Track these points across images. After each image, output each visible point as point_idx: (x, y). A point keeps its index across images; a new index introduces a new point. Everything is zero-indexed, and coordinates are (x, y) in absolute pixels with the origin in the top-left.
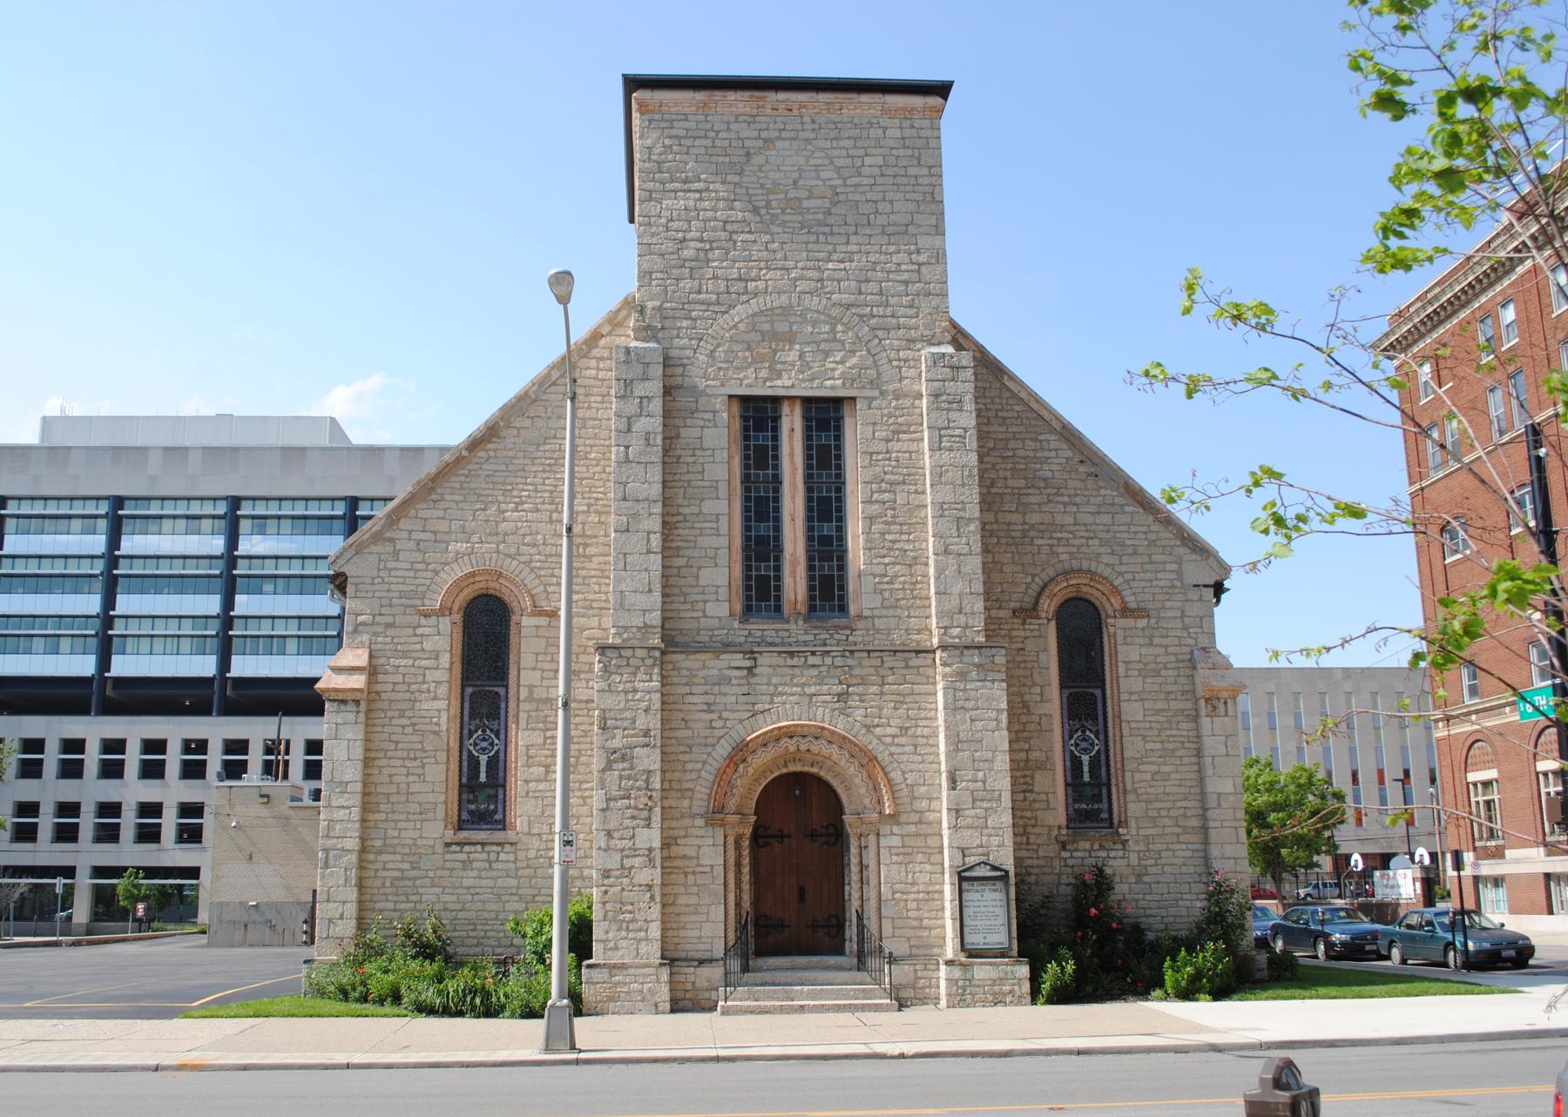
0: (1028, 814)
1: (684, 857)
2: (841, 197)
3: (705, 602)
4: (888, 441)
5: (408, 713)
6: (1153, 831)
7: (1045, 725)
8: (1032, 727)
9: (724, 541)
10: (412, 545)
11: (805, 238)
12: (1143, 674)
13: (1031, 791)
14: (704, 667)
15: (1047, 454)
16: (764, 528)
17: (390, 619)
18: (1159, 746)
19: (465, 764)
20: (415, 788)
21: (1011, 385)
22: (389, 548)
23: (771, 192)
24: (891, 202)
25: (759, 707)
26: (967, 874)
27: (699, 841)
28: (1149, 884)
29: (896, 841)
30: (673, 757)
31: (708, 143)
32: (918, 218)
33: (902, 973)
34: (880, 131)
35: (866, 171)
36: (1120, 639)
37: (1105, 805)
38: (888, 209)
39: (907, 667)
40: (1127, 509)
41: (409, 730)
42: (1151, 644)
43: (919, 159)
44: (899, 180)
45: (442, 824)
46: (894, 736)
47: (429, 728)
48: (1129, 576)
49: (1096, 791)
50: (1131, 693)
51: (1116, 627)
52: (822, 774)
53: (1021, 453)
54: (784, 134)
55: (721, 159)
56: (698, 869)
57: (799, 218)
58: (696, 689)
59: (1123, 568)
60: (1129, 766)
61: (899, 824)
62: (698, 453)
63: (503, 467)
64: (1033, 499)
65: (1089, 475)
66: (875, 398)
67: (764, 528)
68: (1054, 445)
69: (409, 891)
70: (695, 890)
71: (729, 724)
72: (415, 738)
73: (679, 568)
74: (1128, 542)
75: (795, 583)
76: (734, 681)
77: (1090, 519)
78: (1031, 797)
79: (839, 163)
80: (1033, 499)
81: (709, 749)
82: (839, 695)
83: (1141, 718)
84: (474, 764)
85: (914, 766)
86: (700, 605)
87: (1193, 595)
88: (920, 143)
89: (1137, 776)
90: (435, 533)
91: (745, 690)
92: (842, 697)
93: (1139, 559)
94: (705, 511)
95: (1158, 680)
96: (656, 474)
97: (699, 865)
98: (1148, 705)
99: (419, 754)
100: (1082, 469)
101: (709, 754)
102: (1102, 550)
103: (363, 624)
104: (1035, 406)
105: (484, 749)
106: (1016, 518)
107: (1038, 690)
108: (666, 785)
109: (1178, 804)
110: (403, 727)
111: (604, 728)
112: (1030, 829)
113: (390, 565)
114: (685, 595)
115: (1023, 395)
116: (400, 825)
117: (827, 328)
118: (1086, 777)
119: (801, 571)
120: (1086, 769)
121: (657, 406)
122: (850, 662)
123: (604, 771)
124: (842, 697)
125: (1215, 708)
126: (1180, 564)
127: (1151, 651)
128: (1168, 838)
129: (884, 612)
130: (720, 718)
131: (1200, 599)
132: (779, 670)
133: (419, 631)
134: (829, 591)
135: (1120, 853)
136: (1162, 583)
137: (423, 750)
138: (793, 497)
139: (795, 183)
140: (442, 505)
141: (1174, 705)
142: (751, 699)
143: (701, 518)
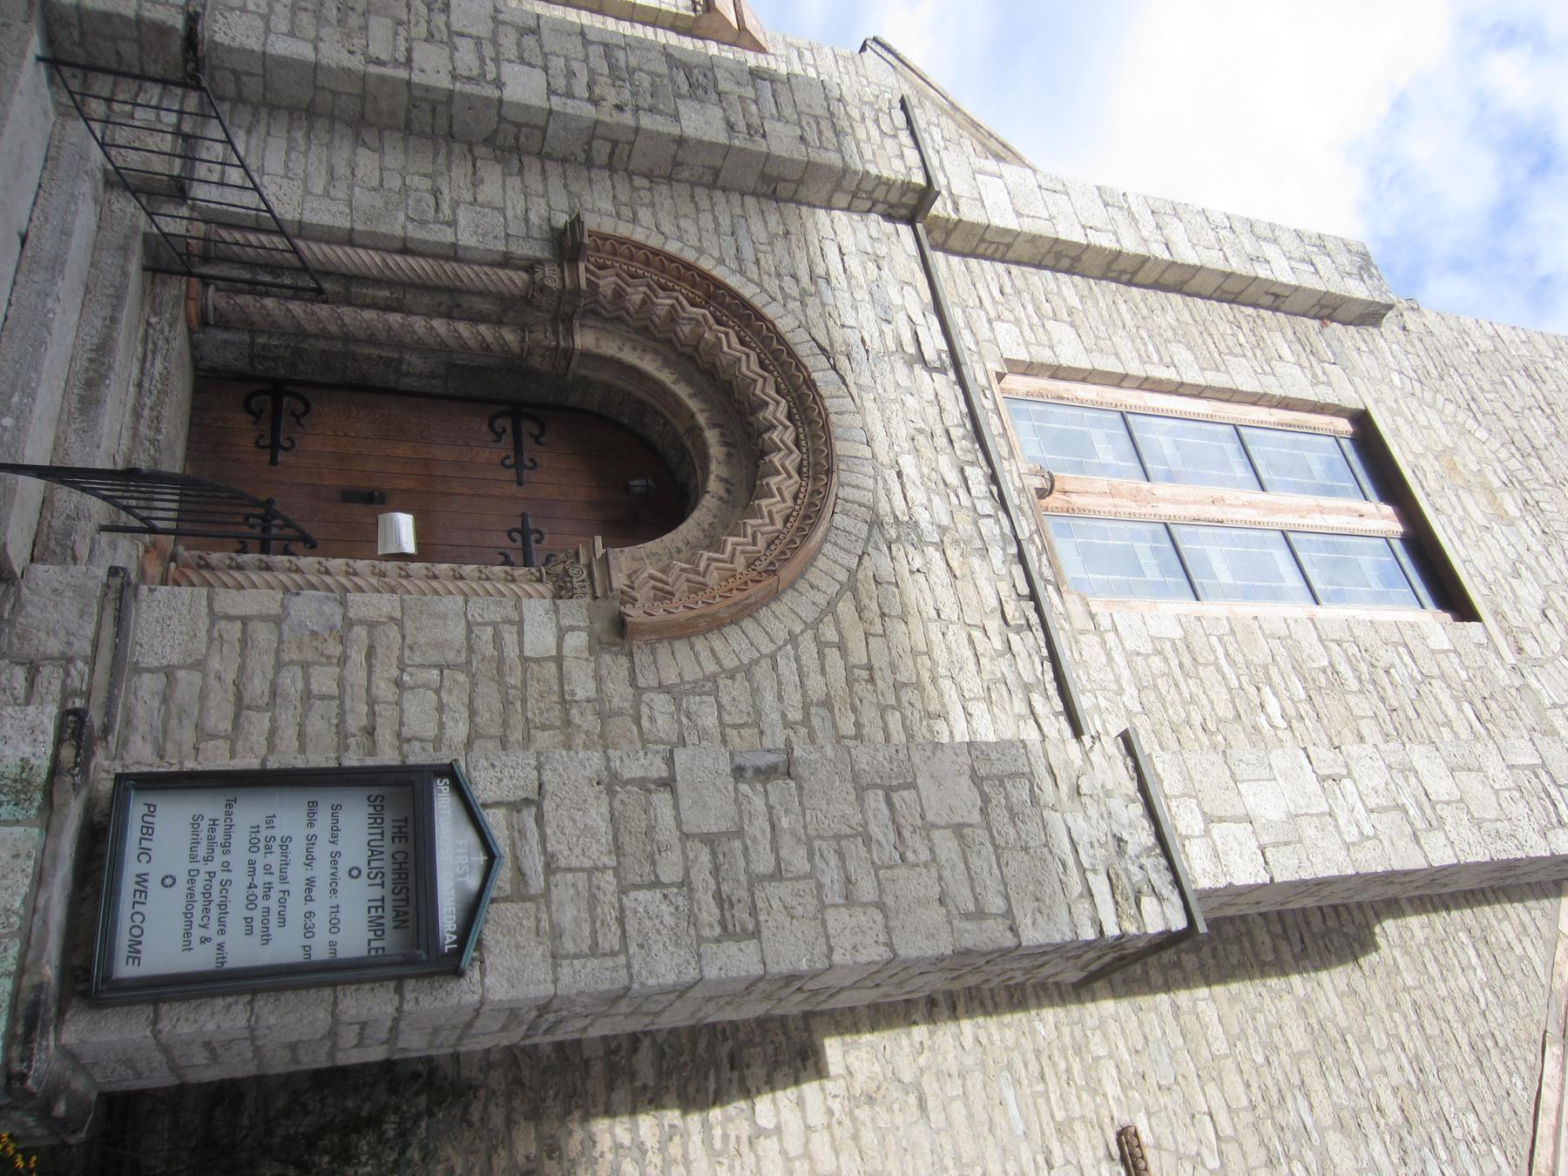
29: (540, 638)
39: (1027, 688)
46: (842, 647)
61: (597, 646)
70: (396, 183)
76: (886, 328)
85: (769, 696)
122: (996, 554)
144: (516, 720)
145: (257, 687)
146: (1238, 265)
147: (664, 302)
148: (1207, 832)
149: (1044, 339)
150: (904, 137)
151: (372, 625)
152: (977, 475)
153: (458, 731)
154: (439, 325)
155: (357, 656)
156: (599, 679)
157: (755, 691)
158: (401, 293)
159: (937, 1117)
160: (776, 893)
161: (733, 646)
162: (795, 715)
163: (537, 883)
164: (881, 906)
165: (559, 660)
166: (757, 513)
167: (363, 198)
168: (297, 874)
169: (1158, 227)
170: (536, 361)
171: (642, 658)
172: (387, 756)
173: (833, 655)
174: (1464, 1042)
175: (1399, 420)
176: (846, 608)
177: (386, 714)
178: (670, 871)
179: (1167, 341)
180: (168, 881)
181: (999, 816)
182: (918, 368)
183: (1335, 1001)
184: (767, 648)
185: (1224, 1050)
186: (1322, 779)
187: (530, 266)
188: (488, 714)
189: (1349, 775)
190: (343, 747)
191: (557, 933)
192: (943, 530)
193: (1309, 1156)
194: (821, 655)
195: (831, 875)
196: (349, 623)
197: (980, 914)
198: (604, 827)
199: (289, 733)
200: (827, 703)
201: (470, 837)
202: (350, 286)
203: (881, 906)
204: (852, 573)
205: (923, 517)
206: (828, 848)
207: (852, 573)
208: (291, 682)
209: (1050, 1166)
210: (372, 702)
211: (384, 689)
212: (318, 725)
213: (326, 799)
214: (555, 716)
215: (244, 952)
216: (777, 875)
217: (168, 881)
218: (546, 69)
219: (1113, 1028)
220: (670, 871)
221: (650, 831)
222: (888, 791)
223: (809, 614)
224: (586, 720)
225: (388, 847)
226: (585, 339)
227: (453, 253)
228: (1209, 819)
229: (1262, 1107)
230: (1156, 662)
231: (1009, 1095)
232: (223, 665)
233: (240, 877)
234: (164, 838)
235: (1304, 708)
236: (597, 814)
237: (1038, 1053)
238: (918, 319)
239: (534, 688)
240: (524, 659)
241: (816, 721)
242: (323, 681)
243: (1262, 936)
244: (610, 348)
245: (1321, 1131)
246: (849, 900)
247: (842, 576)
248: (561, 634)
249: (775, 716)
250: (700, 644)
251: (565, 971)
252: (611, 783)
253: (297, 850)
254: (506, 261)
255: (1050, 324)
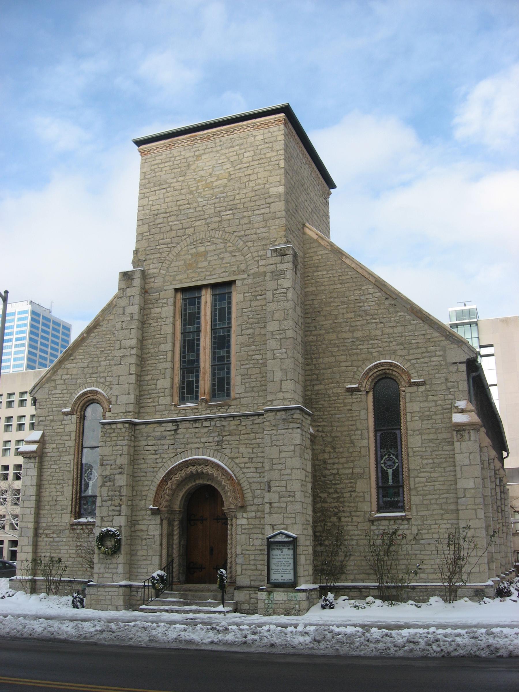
0: (352, 504)
1: (142, 530)
2: (233, 177)
3: (159, 397)
4: (251, 301)
5: (58, 462)
6: (426, 513)
7: (363, 452)
8: (355, 454)
9: (169, 365)
10: (62, 382)
11: (213, 201)
12: (421, 419)
13: (354, 491)
14: (154, 431)
15: (367, 297)
16: (191, 356)
17: (52, 418)
18: (431, 461)
19: (380, 474)
20: (59, 498)
21: (347, 261)
22: (53, 384)
23: (199, 182)
24: (257, 173)
25: (179, 451)
26: (272, 540)
27: (148, 523)
28: (424, 544)
29: (244, 521)
30: (138, 478)
31: (171, 163)
32: (271, 179)
33: (240, 596)
34: (253, 138)
35: (245, 160)
36: (408, 399)
37: (401, 498)
38: (255, 178)
39: (253, 424)
40: (413, 322)
41: (58, 470)
42: (426, 401)
43: (272, 147)
44: (262, 161)
45: (69, 515)
46: (245, 463)
47: (65, 469)
48: (413, 362)
49: (396, 490)
50: (414, 431)
51: (406, 392)
52: (213, 485)
53: (352, 298)
54: (207, 151)
55: (177, 170)
56: (147, 537)
57: (211, 192)
58: (150, 443)
59: (410, 357)
60: (413, 474)
61: (245, 511)
62: (159, 320)
63: (101, 340)
64: (358, 323)
65: (391, 305)
66: (245, 279)
67: (191, 356)
68: (371, 291)
69: (56, 548)
70: (145, 547)
71: (164, 460)
72: (60, 474)
73: (148, 381)
74: (413, 341)
75: (205, 383)
76: (168, 438)
77: (390, 331)
78: (354, 494)
79: (232, 159)
80: (358, 323)
81: (155, 474)
82: (218, 442)
83: (420, 445)
84: (385, 474)
85: (255, 480)
86: (157, 399)
87: (453, 368)
88: (272, 139)
89: (417, 480)
90: (71, 375)
91: (172, 442)
92: (219, 443)
93: (420, 351)
94: (161, 350)
95: (430, 422)
96: (134, 333)
97: (148, 535)
98: (425, 437)
99: (62, 482)
100: (387, 302)
101: (155, 477)
102: (397, 348)
103: (41, 421)
104: (360, 271)
105: (390, 466)
106: (349, 335)
107: (359, 432)
108: (135, 493)
109: (442, 496)
110: (56, 469)
111: (102, 465)
112: (353, 514)
113: (53, 392)
114: (149, 394)
115: (353, 266)
116: (53, 516)
117: (222, 246)
118: (390, 482)
119: (208, 376)
120: (390, 477)
121: (137, 300)
122: (224, 423)
123: (101, 487)
124: (219, 443)
125: (462, 436)
126: (445, 351)
127: (426, 404)
128: (436, 517)
129: (246, 395)
130: (160, 457)
131: (457, 371)
132: (189, 430)
133: (64, 422)
134: (221, 386)
135: (406, 527)
136: (434, 363)
137: (63, 480)
138: (205, 338)
139: (210, 174)
140: (75, 361)
141: (440, 436)
142: (175, 446)
143: (159, 354)
144: (259, 526)
145: (253, 567)
146: (135, 325)
147: (168, 491)
148: (283, 392)
149: (163, 390)
150: (114, 426)
151: (242, 550)
152: (206, 424)
153: (261, 536)
154: (175, 538)
155: (247, 552)
156: (252, 511)
157: (254, 482)
158: (170, 545)
159: (339, 434)
160: (289, 488)
161: (245, 485)
162: (258, 475)
163: (285, 526)
164: (292, 469)
165: (248, 518)
166: (217, 477)
167: (151, 553)
168: (282, 560)
169: (126, 348)
170: (180, 517)
171: (247, 503)
172: (266, 547)
173: (247, 465)
174: (341, 286)
175: (177, 278)
176: (237, 461)
177: (258, 548)
178: (284, 505)
179: (159, 351)
180: (282, 576)
181: (278, 443)
182: (178, 432)
183: (327, 322)
184: (245, 479)
185: (334, 358)
186: (274, 359)
187: (162, 520)
188: (258, 531)
189: (273, 350)
190: (263, 554)
191: (292, 524)
192: (219, 435)
193: (358, 343)
194: (247, 468)
195: (287, 477)
196: (242, 554)
197: (294, 451)
198: (277, 515)
199: (262, 562)
200: (256, 468)
201: (278, 536)
202: (169, 555)
203: (292, 469)
204: (229, 458)
205: (216, 439)
206: (282, 477)
207: (229, 458)
208: (252, 562)
209: (351, 410)
210: (256, 550)
211: (254, 548)
212: (260, 558)
213: (271, 556)
214: (258, 520)
215: (292, 566)
216: (286, 487)
217: (282, 576)
218: (113, 516)
219: (327, 386)
220: (284, 505)
221: (278, 507)
222: (273, 464)
223: (238, 469)
224: (259, 514)
225: (279, 548)
226: (177, 508)
227: (161, 535)
228: (281, 391)
229: (346, 352)
230: (247, 385)
231: (337, 416)
232: (250, 573)
233: (282, 567)
234: (276, 577)
235: (258, 348)
236: (275, 516)
237: (330, 407)
238: (164, 429)
239: (253, 523)
240: (248, 524)
241: (260, 471)
242: (252, 557)
243: (311, 338)
244: (178, 502)
245: (353, 338)
246: (290, 475)
247: (230, 460)
248: (243, 517)
249: (259, 479)
250: (245, 492)
251: (297, 522)
252: (270, 513)
253: (279, 560)
254: (161, 524)
255: (158, 387)
